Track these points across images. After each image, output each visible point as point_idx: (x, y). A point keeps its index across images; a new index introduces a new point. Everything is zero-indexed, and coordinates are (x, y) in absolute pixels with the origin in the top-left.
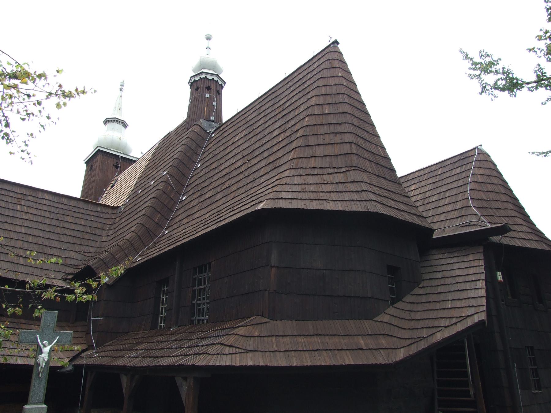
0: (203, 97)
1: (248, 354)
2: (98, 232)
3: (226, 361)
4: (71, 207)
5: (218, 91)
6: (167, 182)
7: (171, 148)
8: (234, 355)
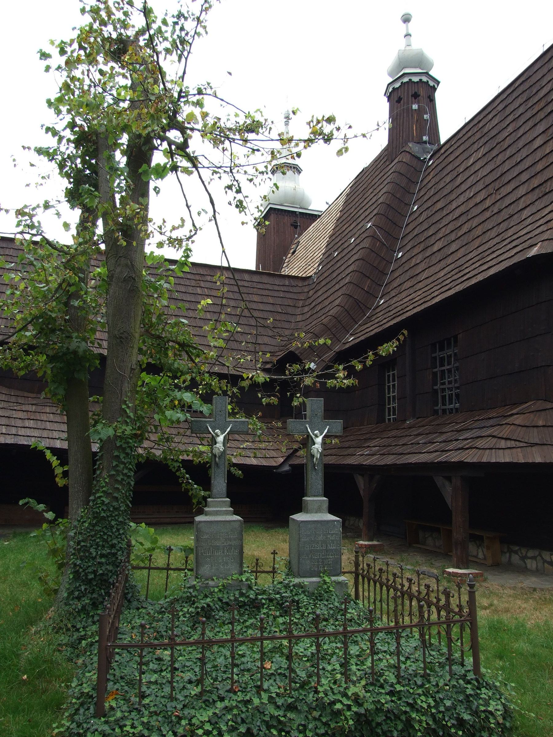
0: (409, 110)
1: (534, 448)
2: (290, 310)
3: (505, 457)
4: (255, 284)
5: (429, 97)
6: (374, 237)
7: (371, 190)
8: (514, 450)
